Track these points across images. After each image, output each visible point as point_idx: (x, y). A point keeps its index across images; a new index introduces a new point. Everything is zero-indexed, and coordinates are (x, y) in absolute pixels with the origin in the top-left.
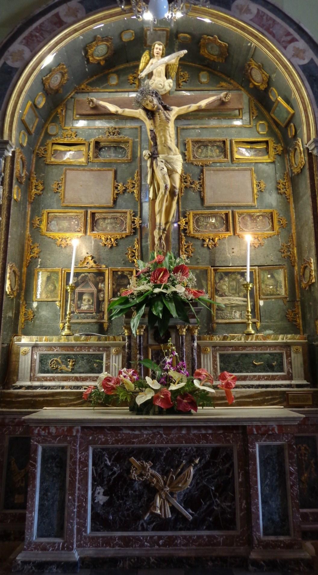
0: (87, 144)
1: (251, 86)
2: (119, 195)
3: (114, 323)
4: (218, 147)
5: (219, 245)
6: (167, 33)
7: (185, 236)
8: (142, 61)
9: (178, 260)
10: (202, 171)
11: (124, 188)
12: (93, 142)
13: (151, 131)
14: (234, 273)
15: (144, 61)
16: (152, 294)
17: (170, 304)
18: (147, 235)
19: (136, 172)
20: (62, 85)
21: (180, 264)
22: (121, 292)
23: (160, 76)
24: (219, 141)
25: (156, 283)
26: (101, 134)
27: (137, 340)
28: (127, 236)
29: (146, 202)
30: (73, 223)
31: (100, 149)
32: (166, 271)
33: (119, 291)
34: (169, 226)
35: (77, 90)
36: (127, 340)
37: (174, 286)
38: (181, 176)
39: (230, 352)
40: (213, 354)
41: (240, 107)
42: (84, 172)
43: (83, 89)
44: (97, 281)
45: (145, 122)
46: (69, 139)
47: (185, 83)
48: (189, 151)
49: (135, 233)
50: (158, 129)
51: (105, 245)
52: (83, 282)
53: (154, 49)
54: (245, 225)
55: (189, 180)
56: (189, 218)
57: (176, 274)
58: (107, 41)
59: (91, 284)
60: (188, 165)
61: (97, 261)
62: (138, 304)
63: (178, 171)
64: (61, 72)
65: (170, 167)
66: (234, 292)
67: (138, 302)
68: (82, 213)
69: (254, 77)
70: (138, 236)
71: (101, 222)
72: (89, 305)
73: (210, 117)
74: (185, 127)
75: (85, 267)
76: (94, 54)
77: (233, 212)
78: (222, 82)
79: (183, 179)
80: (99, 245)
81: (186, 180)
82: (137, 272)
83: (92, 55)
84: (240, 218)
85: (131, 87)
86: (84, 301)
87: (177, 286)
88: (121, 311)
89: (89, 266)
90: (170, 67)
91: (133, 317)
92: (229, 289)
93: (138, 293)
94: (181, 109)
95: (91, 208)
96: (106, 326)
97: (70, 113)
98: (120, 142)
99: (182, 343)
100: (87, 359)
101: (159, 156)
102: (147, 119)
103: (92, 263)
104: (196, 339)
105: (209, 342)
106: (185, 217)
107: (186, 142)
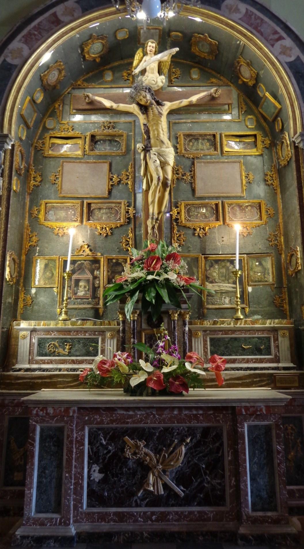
0: (83, 137)
1: (240, 82)
2: (114, 186)
3: (109, 308)
4: (209, 140)
5: (209, 234)
6: (160, 32)
7: (177, 225)
8: (135, 58)
9: (170, 249)
10: (193, 164)
11: (119, 180)
12: (89, 136)
13: (144, 125)
14: (223, 260)
15: (138, 58)
16: (146, 280)
17: (162, 290)
18: (140, 224)
19: (130, 164)
20: (60, 82)
21: (172, 252)
22: (115, 278)
23: (153, 73)
24: (210, 135)
25: (149, 270)
26: (97, 128)
27: (131, 325)
28: (121, 226)
29: (139, 193)
30: (69, 213)
31: (96, 143)
32: (158, 259)
33: (113, 278)
34: (162, 216)
35: (74, 86)
36: (121, 324)
37: (166, 273)
38: (173, 168)
39: (220, 336)
40: (203, 338)
41: (230, 102)
42: (80, 165)
43: (79, 85)
44: (93, 269)
45: (138, 116)
46: (66, 132)
47: (177, 80)
48: (181, 144)
49: (129, 223)
50: (151, 123)
51: (101, 234)
52: (79, 270)
53: (147, 46)
54: (235, 214)
55: (181, 172)
56: (180, 208)
57: (168, 262)
58: (102, 39)
59: (87, 271)
60: (180, 158)
61: (92, 249)
62: (132, 290)
63: (170, 163)
64: (58, 69)
65: (163, 159)
66: (224, 279)
67: (132, 288)
68: (78, 203)
69: (243, 73)
70: (132, 225)
71: (96, 212)
72: (85, 291)
73: (200, 112)
74: (177, 121)
75: (82, 255)
76: (90, 52)
77: (222, 202)
78: (212, 78)
79: (175, 171)
80: (94, 234)
81: (178, 172)
82: (131, 259)
83: (88, 53)
84: (229, 209)
85: (125, 84)
86: (80, 287)
87: (169, 273)
88: (116, 297)
89: (85, 254)
90: (162, 64)
91: (127, 303)
92: (219, 276)
93: (132, 280)
94: (173, 104)
95: (87, 198)
96: (101, 311)
97: (67, 107)
98: (115, 136)
99: (174, 328)
100: (83, 343)
101: (152, 149)
102: (140, 113)
103: (88, 251)
104: (187, 323)
105: (199, 327)
106: (177, 207)
107: (178, 136)
